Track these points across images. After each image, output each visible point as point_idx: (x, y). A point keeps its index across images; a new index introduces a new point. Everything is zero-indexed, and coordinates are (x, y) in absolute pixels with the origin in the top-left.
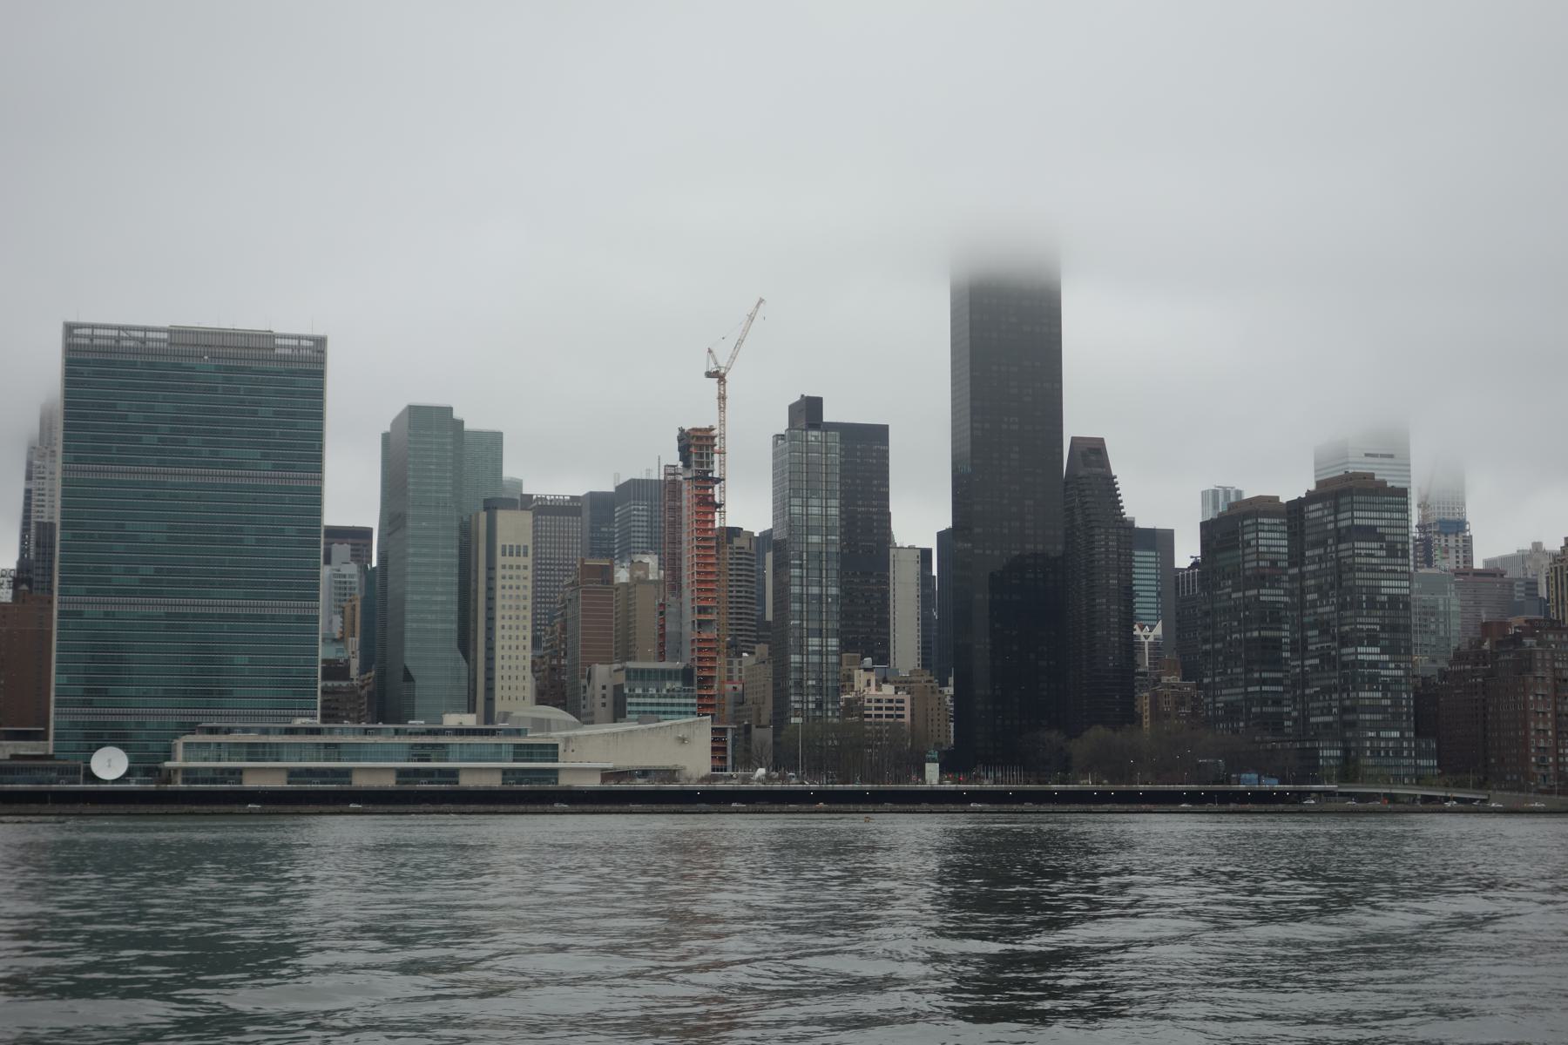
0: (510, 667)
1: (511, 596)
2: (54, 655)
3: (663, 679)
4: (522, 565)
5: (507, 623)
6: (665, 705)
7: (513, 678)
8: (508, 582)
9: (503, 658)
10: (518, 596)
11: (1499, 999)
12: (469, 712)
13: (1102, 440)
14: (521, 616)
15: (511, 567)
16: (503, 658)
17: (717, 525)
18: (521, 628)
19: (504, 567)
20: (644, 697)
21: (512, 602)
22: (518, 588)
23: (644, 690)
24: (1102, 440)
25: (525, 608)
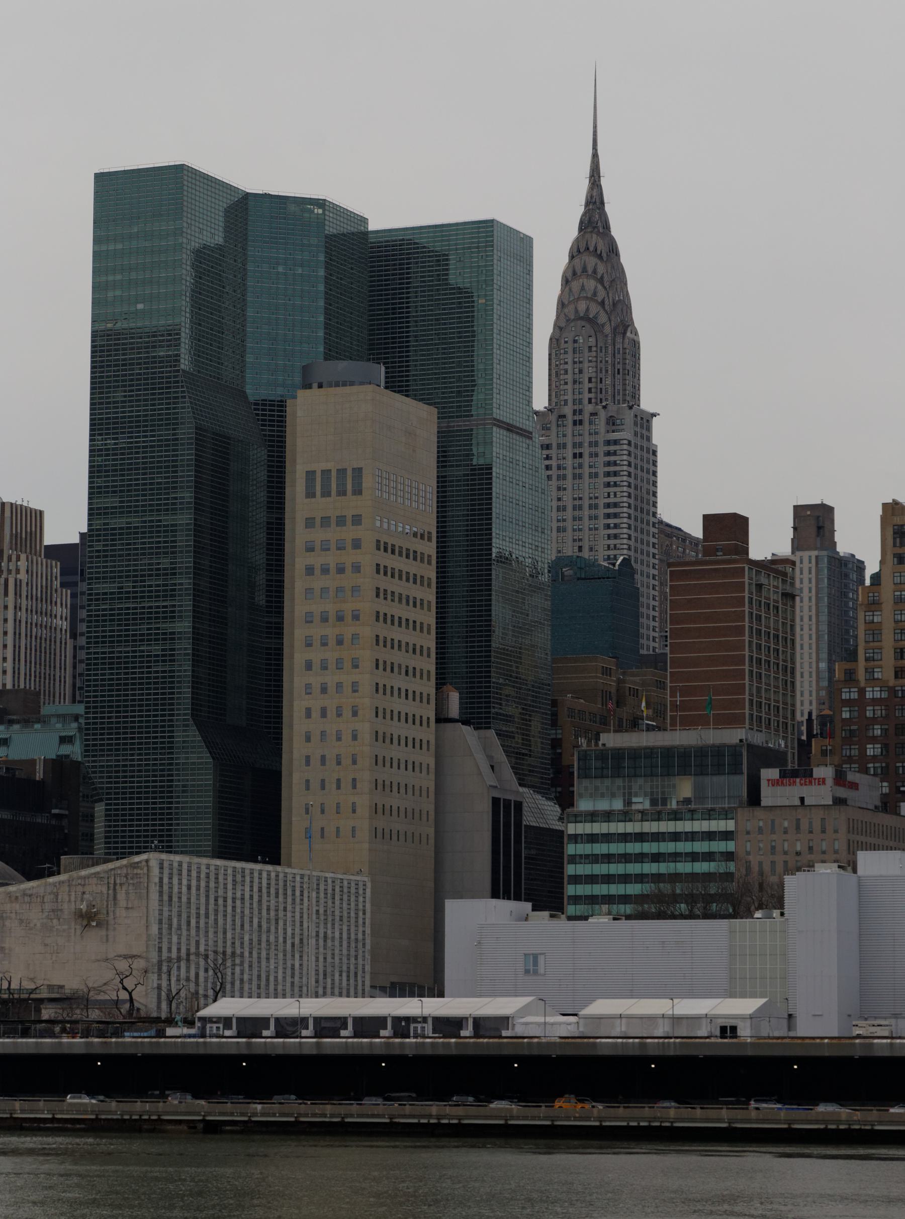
0: (323, 759)
1: (324, 590)
2: (523, 881)
3: (668, 772)
4: (349, 513)
5: (316, 655)
6: (657, 837)
7: (331, 786)
8: (317, 560)
9: (308, 739)
10: (339, 590)
11: (135, 953)
12: (495, 895)
13: (41, 513)
14: (347, 638)
15: (325, 521)
16: (308, 739)
17: (474, 462)
18: (347, 665)
19: (310, 523)
20: (658, 817)
21: (330, 608)
22: (341, 570)
23: (654, 802)
24: (41, 513)
25: (356, 617)
